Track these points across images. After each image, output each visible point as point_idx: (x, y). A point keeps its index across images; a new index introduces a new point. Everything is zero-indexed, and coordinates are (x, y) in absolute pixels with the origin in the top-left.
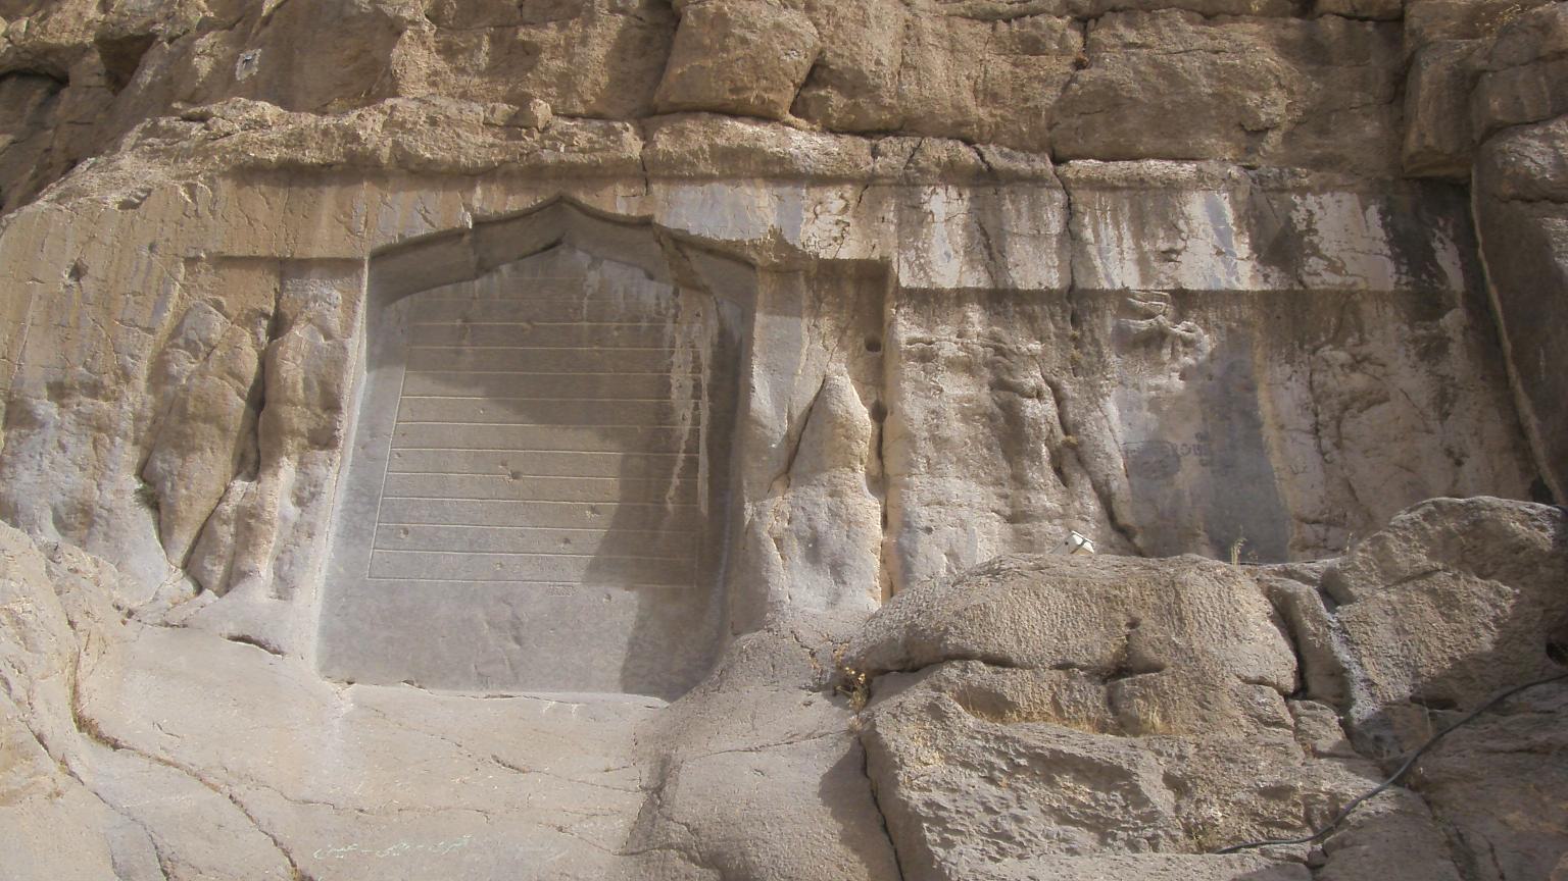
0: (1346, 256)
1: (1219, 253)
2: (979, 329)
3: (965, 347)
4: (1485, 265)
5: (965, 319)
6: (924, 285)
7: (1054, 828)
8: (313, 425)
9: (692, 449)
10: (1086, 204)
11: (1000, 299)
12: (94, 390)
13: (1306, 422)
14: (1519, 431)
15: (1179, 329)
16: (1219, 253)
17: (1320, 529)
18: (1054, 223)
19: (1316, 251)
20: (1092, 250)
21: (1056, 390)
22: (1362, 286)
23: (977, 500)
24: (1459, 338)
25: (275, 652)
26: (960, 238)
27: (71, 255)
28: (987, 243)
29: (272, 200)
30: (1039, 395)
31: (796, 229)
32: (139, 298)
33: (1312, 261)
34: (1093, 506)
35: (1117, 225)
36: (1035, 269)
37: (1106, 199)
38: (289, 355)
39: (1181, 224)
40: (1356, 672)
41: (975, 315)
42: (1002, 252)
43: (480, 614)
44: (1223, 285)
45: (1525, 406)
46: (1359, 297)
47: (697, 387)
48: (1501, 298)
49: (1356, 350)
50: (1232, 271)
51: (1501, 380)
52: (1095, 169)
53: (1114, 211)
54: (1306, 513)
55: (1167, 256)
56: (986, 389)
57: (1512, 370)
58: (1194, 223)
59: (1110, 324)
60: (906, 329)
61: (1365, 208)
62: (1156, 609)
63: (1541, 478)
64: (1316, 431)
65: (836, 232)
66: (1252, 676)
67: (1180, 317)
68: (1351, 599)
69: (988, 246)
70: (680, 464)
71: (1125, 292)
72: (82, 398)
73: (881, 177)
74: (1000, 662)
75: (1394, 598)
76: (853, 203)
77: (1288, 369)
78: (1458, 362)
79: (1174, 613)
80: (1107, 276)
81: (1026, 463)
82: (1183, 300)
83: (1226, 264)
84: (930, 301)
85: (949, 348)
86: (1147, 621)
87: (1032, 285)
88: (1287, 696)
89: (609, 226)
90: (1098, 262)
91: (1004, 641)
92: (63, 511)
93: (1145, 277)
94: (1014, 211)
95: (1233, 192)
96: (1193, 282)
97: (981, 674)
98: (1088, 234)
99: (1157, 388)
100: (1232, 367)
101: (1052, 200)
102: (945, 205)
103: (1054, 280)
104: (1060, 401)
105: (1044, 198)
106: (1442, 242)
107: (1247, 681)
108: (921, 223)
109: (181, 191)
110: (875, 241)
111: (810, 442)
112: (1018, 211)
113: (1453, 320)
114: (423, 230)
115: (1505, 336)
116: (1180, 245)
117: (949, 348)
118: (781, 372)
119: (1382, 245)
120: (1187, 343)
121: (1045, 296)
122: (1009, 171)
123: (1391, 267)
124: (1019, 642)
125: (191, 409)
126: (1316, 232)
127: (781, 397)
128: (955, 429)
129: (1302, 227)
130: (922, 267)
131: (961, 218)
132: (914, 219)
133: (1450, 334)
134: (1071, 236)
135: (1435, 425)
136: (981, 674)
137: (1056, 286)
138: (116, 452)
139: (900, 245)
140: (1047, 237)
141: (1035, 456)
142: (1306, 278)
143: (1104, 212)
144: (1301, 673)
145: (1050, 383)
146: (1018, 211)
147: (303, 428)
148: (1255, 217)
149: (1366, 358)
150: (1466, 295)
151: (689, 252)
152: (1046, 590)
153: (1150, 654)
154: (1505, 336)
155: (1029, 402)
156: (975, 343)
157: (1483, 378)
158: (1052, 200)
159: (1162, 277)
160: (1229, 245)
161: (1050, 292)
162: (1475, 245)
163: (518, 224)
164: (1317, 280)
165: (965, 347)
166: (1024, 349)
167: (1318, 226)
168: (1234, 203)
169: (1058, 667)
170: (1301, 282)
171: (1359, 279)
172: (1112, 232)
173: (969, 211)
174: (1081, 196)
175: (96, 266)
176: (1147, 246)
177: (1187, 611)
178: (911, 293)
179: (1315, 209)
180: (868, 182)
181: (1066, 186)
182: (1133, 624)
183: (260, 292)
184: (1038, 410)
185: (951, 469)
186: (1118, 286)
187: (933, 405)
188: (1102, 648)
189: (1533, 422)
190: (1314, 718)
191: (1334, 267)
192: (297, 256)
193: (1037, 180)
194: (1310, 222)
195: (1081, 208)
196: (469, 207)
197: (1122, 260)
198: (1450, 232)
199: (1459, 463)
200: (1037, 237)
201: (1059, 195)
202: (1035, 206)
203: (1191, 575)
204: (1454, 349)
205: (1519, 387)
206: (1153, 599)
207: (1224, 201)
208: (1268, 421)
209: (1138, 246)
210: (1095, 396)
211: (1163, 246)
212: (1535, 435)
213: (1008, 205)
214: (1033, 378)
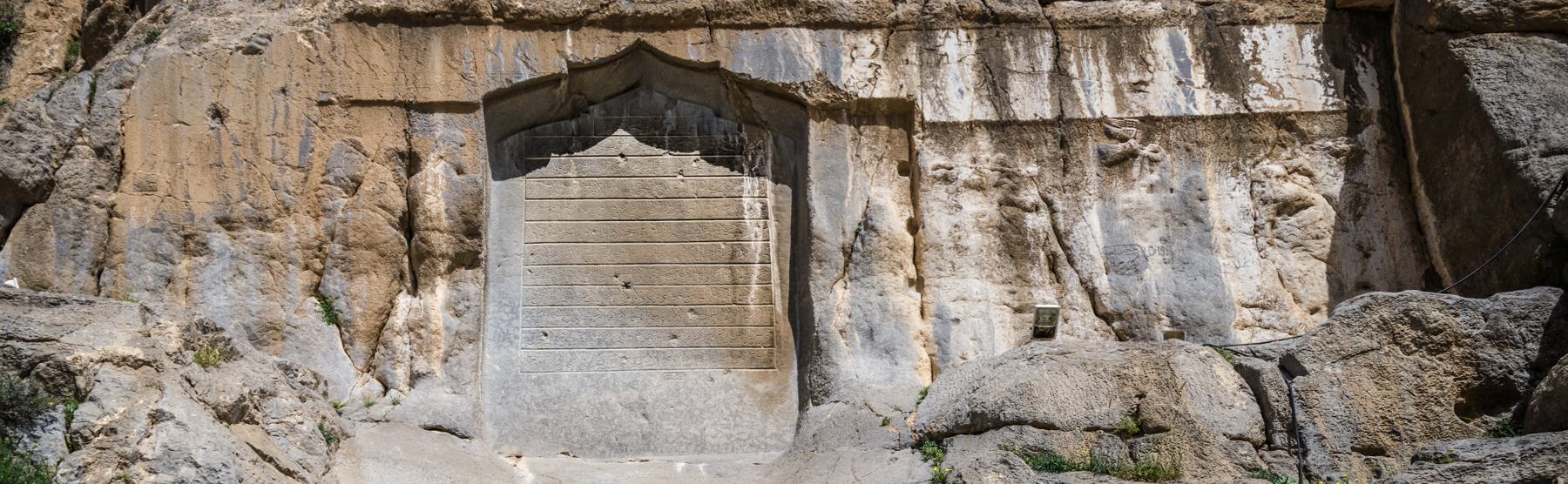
0: (1284, 82)
1: (1180, 83)
2: (988, 155)
3: (978, 171)
4: (1401, 87)
5: (976, 148)
6: (944, 119)
7: (63, 295)
8: (458, 249)
9: (765, 261)
10: (1071, 43)
11: (1005, 129)
12: (262, 223)
13: (1248, 226)
14: (1417, 228)
15: (1147, 151)
16: (1180, 83)
17: (1257, 312)
18: (1046, 63)
19: (1259, 79)
20: (1076, 83)
21: (1049, 204)
22: (1296, 108)
23: (992, 296)
24: (1373, 150)
25: (463, 437)
26: (971, 76)
27: (210, 99)
28: (993, 78)
29: (387, 46)
30: (1037, 208)
31: (837, 73)
32: (284, 140)
33: (1257, 86)
34: (1082, 300)
35: (1097, 61)
36: (1031, 101)
37: (1087, 38)
38: (429, 189)
39: (1149, 58)
40: (1310, 429)
41: (983, 141)
42: (1005, 88)
43: (614, 400)
44: (1183, 111)
45: (1425, 207)
46: (1293, 117)
47: (764, 208)
48: (1413, 116)
49: (1288, 163)
50: (1190, 98)
51: (1406, 188)
52: (1077, 9)
53: (1094, 47)
54: (1245, 300)
55: (1137, 87)
56: (996, 206)
57: (1417, 179)
58: (1160, 57)
59: (1091, 147)
60: (931, 158)
61: (1301, 38)
62: (1158, 384)
63: (1433, 267)
64: (1256, 230)
65: (870, 73)
66: (1235, 433)
67: (1147, 139)
68: (1304, 373)
69: (994, 84)
70: (757, 272)
71: (1103, 120)
72: (251, 231)
73: (904, 23)
74: (1050, 427)
75: (1338, 371)
76: (882, 47)
77: (1233, 181)
78: (1371, 171)
79: (1170, 386)
80: (1089, 107)
81: (1029, 265)
82: (1150, 124)
83: (1186, 93)
84: (946, 132)
85: (965, 173)
86: (1152, 392)
87: (1029, 117)
88: (1257, 447)
89: (680, 71)
90: (1081, 95)
91: (1044, 411)
92: (254, 329)
93: (1121, 106)
94: (1014, 53)
95: (1192, 28)
96: (1158, 111)
97: (1033, 436)
98: (1073, 70)
99: (1129, 201)
100: (1189, 181)
101: (1043, 41)
102: (957, 46)
103: (1048, 113)
104: (1053, 212)
105: (1037, 39)
106: (1363, 65)
107: (1232, 438)
108: (938, 64)
109: (300, 38)
110: (902, 81)
111: (860, 250)
112: (1017, 52)
113: (1369, 135)
114: (526, 76)
115: (1413, 149)
116: (1148, 77)
117: (965, 173)
118: (836, 196)
119: (1314, 71)
120: (1152, 161)
121: (1039, 125)
122: (1008, 14)
123: (1320, 89)
124: (1059, 411)
125: (351, 239)
126: (1259, 61)
127: (836, 215)
128: (974, 240)
129: (1248, 57)
130: (941, 104)
131: (971, 59)
132: (932, 60)
133: (1367, 147)
134: (1059, 74)
135: (1350, 225)
136: (1033, 436)
137: (1049, 116)
138: (292, 277)
139: (922, 85)
140: (1040, 73)
141: (1034, 259)
142: (1250, 103)
143: (1086, 49)
144: (1268, 429)
145: (1045, 200)
146: (1017, 52)
147: (451, 252)
148: (1210, 49)
149: (1296, 170)
150: (1381, 112)
151: (750, 94)
152: (1071, 371)
153: (1157, 418)
154: (1413, 149)
155: (1029, 216)
156: (986, 168)
157: (1390, 184)
158: (1043, 41)
159: (1134, 106)
160: (1188, 75)
161: (1044, 122)
162: (1393, 69)
163: (604, 69)
164: (1259, 104)
165: (978, 171)
166: (1023, 172)
167: (1262, 56)
168: (1193, 36)
169: (1088, 430)
170: (1246, 107)
171: (1293, 102)
172: (1093, 67)
173: (977, 52)
174: (1066, 35)
175: (235, 112)
176: (1121, 79)
177: (1180, 382)
178: (934, 125)
179: (1260, 40)
180: (895, 25)
181: (1054, 26)
182: (1141, 396)
183: (382, 133)
184: (1037, 222)
185: (973, 272)
186: (1098, 115)
187: (955, 220)
188: (1113, 411)
189: (1430, 220)
190: (1282, 464)
191: (1274, 92)
192: (420, 100)
193: (1031, 22)
194: (1255, 53)
195: (1067, 47)
196: (561, 53)
197: (1101, 92)
198: (1371, 56)
199: (1367, 256)
200: (1033, 73)
201: (1048, 36)
202: (1030, 46)
203: (1181, 357)
204: (1368, 160)
205: (1422, 193)
206: (1154, 376)
207: (1184, 34)
208: (1217, 225)
209: (1114, 79)
210: (1079, 209)
211: (1134, 78)
212: (1432, 233)
213: (1009, 46)
214: (1030, 195)
